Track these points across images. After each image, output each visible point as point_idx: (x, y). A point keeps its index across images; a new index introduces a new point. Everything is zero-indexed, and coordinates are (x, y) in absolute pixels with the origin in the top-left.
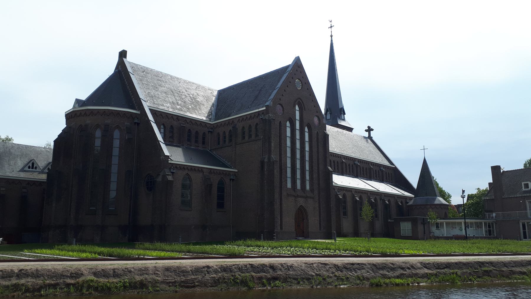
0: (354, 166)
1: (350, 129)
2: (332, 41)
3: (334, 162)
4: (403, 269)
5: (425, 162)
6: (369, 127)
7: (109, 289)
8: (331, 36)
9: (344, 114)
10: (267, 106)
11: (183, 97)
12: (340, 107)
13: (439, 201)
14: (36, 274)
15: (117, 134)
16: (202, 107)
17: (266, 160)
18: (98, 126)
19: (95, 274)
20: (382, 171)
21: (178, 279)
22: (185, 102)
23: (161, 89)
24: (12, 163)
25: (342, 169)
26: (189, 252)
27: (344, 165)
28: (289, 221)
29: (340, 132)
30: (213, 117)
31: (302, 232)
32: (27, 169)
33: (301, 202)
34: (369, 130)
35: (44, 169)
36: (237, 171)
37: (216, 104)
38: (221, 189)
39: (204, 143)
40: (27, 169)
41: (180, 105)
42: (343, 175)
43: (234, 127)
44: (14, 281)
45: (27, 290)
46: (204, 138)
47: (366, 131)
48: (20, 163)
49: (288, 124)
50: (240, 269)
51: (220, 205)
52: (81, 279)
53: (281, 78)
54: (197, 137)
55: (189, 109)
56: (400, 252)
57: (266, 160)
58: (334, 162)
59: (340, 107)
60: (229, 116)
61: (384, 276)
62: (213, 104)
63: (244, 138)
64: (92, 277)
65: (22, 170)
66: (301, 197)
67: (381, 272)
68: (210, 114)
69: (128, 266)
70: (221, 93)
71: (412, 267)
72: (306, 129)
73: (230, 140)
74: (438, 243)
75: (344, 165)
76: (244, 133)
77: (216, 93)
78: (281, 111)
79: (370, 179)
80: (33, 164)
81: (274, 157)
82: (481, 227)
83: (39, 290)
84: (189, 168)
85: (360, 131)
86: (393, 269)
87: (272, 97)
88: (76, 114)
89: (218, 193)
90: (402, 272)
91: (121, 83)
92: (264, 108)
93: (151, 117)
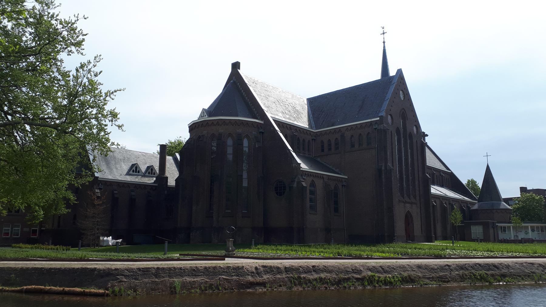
2: (384, 47)
5: (488, 168)
8: (384, 42)
10: (381, 117)
15: (246, 143)
17: (383, 168)
18: (230, 135)
21: (433, 275)
23: (271, 99)
36: (347, 177)
40: (131, 172)
43: (343, 136)
48: (125, 167)
51: (336, 210)
57: (383, 168)
60: (333, 126)
66: (408, 203)
69: (197, 266)
73: (337, 148)
77: (306, 102)
78: (374, 122)
80: (136, 168)
84: (314, 175)
88: (213, 123)
92: (378, 119)
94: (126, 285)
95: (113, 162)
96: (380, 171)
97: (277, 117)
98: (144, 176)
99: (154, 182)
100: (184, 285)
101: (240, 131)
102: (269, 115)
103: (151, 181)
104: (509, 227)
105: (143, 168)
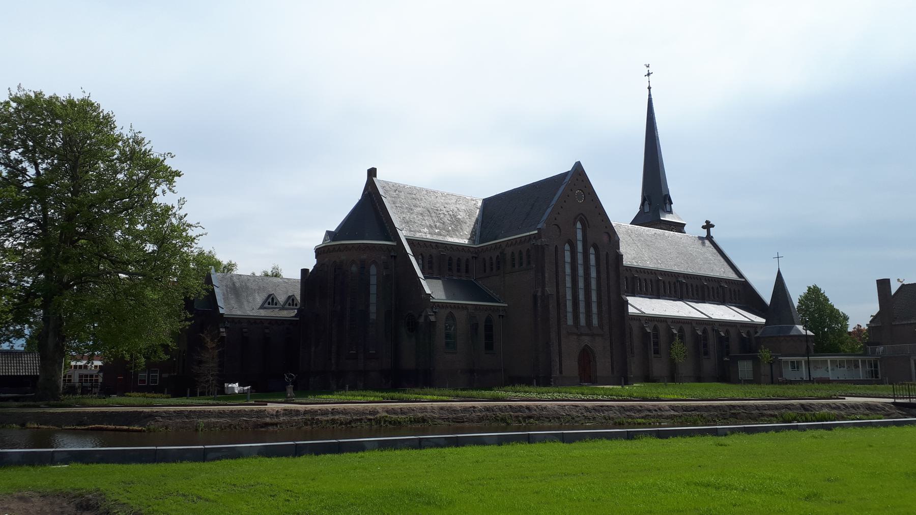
0: (678, 285)
1: (679, 227)
2: (650, 95)
3: (645, 280)
4: (650, 411)
5: (779, 274)
6: (707, 222)
7: (400, 423)
8: (649, 88)
9: (671, 203)
10: (539, 230)
11: (442, 216)
12: (664, 193)
13: (798, 330)
14: (344, 412)
15: (373, 270)
16: (463, 225)
17: (539, 294)
19: (387, 412)
20: (723, 287)
22: (444, 223)
24: (250, 299)
25: (658, 290)
26: (457, 396)
27: (662, 285)
28: (571, 365)
29: (659, 235)
30: (477, 238)
31: (587, 375)
32: (266, 305)
33: (586, 340)
34: (708, 226)
35: (285, 304)
37: (480, 220)
38: (489, 328)
39: (467, 271)
40: (266, 305)
41: (439, 228)
42: (659, 298)
44: (330, 417)
45: (341, 423)
46: (467, 266)
47: (704, 227)
48: (259, 299)
49: (567, 247)
50: (500, 409)
51: (489, 346)
52: (378, 416)
53: (558, 189)
54: (459, 265)
55: (448, 231)
56: (661, 396)
57: (539, 294)
58: (645, 280)
59: (664, 193)
61: (629, 417)
62: (477, 220)
63: (514, 266)
64: (385, 414)
65: (262, 307)
67: (628, 413)
68: (473, 233)
70: (486, 202)
71: (660, 409)
72: (592, 250)
73: (498, 268)
74: (791, 390)
75: (662, 285)
76: (513, 259)
77: (480, 204)
79: (703, 300)
81: (550, 289)
82: (857, 366)
83: (350, 422)
85: (694, 229)
86: (639, 411)
87: (545, 217)
89: (486, 331)
90: (648, 413)
91: (371, 210)
93: (408, 250)
94: (160, 424)
95: (244, 294)
96: (535, 297)
97: (418, 235)
98: (283, 308)
99: (295, 316)
100: (208, 425)
101: (364, 257)
102: (403, 234)
103: (291, 314)
104: (799, 362)
105: (281, 299)
